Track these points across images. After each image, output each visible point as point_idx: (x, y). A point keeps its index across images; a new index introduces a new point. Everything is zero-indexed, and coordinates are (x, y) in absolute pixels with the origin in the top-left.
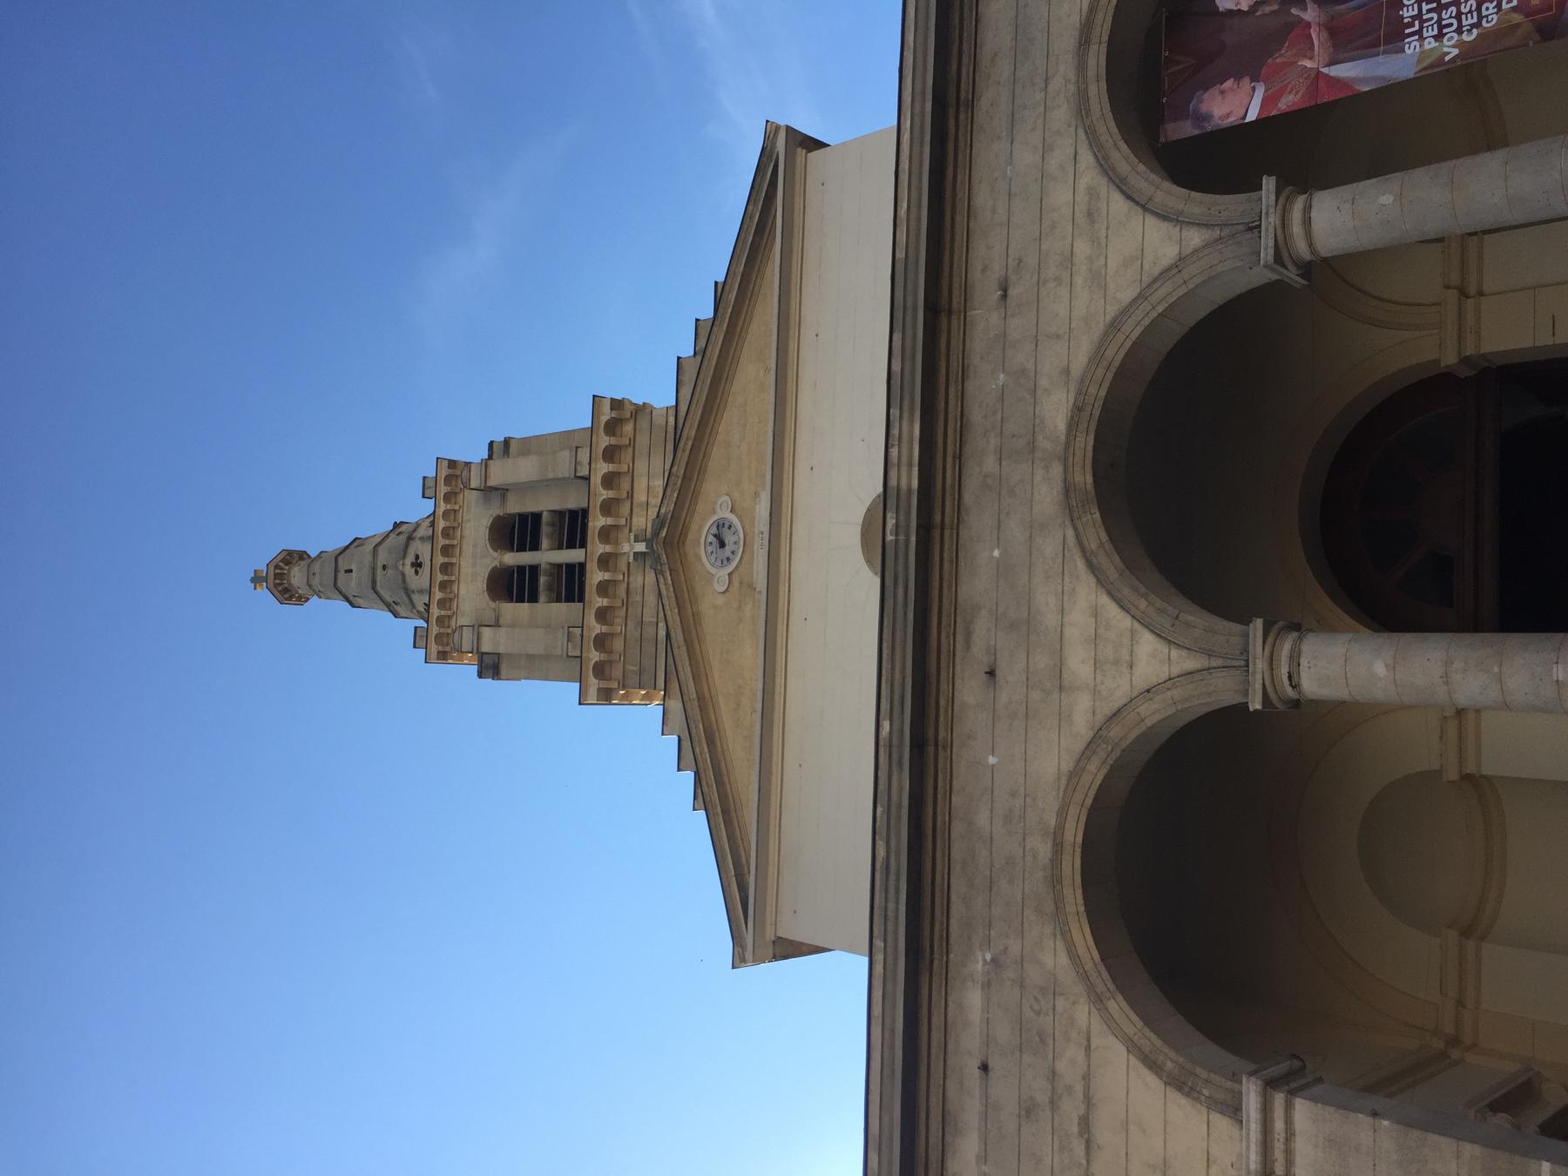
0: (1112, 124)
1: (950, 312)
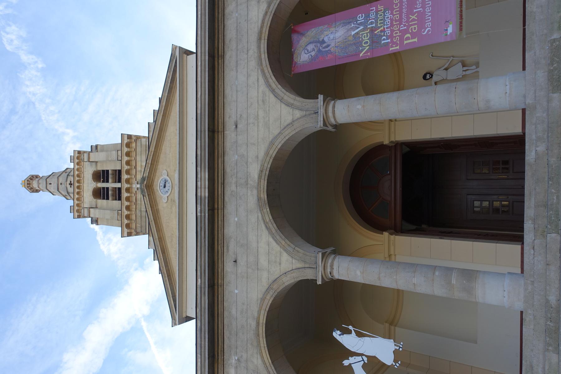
0: (269, 69)
1: (218, 132)
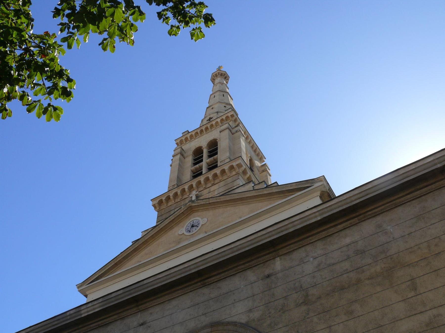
1: (138, 306)
